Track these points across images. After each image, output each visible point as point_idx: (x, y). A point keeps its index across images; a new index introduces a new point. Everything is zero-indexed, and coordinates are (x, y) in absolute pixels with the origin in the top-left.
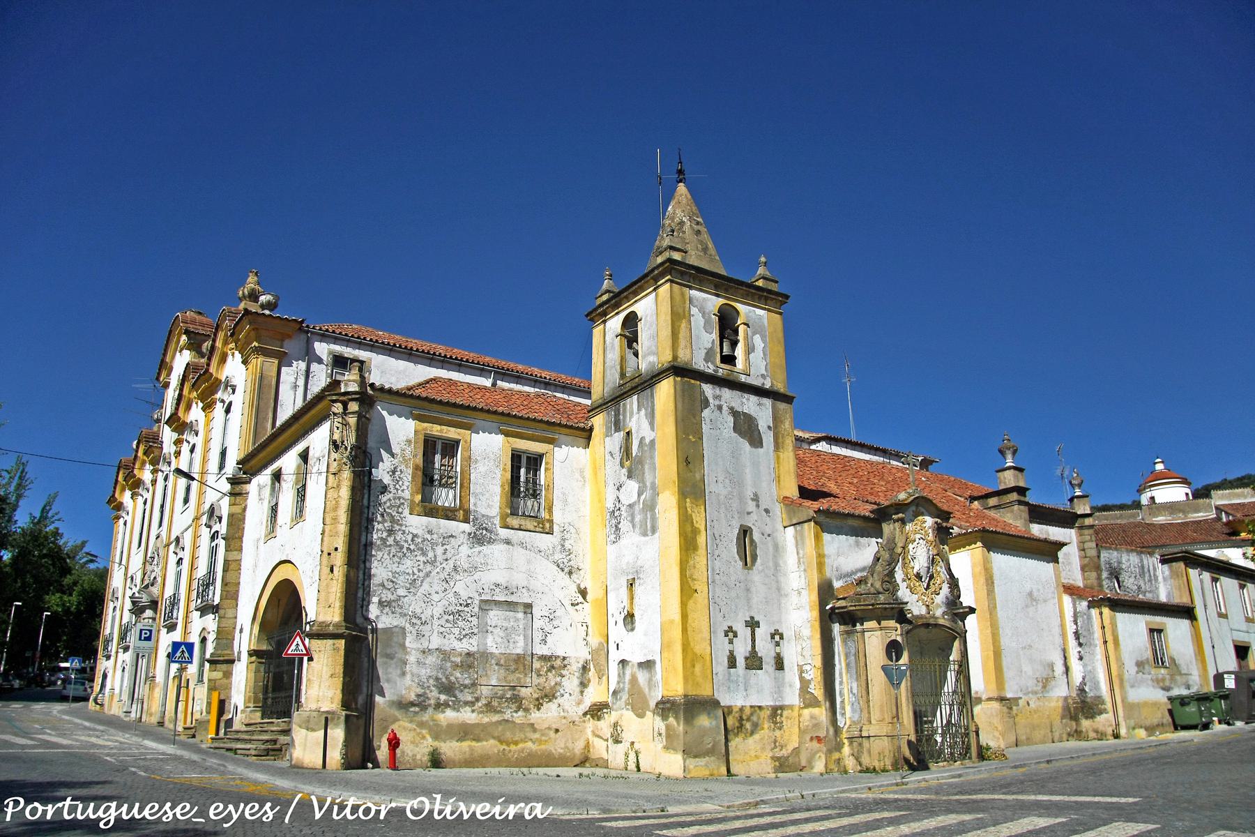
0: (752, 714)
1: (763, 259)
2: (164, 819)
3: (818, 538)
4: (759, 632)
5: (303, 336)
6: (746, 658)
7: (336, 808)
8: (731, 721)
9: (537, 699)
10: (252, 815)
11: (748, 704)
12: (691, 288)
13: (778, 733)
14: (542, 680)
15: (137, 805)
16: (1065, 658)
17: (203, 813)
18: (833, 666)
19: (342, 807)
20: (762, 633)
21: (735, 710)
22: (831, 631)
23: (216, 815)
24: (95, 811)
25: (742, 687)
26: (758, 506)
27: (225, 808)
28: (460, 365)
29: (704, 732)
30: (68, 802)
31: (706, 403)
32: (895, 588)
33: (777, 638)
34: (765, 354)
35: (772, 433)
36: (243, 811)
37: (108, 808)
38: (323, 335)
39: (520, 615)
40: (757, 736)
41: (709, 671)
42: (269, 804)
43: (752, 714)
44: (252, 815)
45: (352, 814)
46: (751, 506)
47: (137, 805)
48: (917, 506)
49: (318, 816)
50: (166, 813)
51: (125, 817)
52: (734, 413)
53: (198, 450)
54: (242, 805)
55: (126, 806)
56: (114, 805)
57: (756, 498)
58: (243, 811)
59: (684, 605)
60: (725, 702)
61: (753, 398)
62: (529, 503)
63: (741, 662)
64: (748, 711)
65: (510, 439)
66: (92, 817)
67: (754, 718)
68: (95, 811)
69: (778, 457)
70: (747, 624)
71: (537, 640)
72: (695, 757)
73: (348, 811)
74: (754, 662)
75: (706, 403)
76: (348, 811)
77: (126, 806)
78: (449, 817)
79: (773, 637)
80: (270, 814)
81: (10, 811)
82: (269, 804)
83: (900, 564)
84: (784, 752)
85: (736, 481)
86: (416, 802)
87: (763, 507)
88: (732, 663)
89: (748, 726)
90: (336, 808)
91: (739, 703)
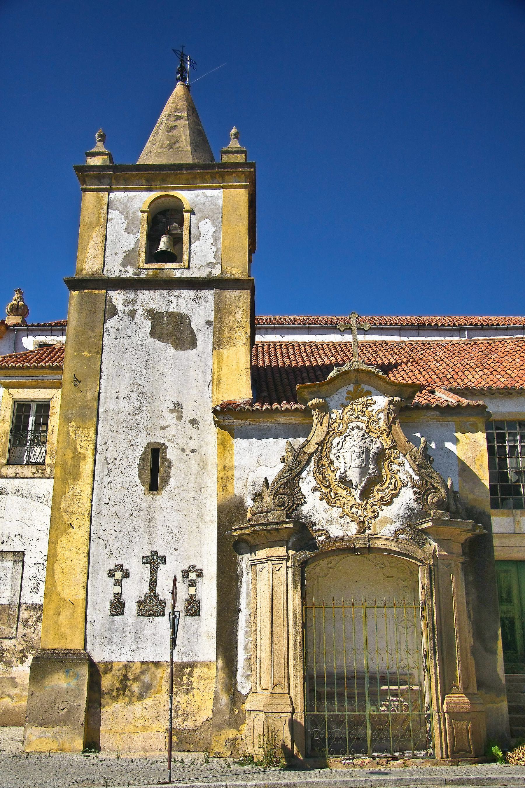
0: (143, 673)
1: (233, 131)
3: (223, 445)
4: (163, 571)
5: (12, 335)
6: (140, 603)
8: (107, 682)
9: (22, 651)
11: (138, 658)
12: (110, 191)
13: (182, 698)
14: (29, 631)
16: (520, 586)
18: (237, 611)
20: (166, 574)
21: (116, 667)
22: (236, 564)
25: (130, 638)
26: (180, 418)
28: (52, 330)
29: (58, 694)
31: (112, 311)
32: (298, 500)
33: (192, 576)
34: (215, 239)
35: (211, 329)
38: (308, 328)
39: (10, 564)
40: (148, 701)
41: (81, 619)
43: (143, 673)
46: (170, 419)
48: (357, 383)
52: (153, 315)
57: (178, 409)
59: (52, 542)
60: (98, 656)
61: (187, 294)
62: (37, 450)
63: (131, 607)
64: (137, 669)
65: (12, 391)
67: (147, 678)
69: (220, 356)
70: (145, 560)
71: (26, 588)
72: (40, 725)
74: (151, 606)
75: (112, 311)
79: (111, 574)
83: (311, 467)
84: (190, 724)
85: (143, 393)
87: (188, 415)
88: (118, 607)
89: (135, 687)
91: (124, 659)
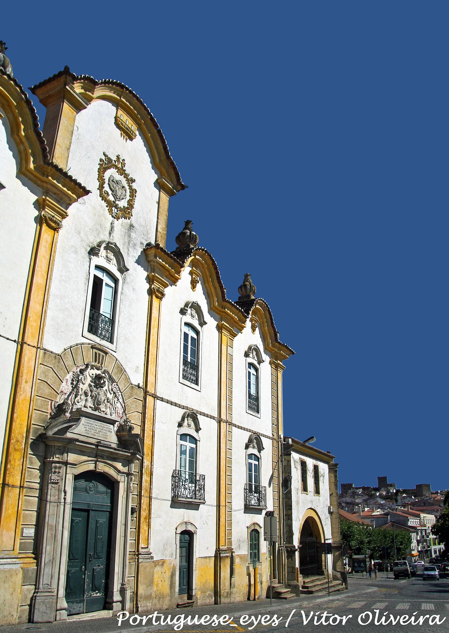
2: (273, 625)
7: (316, 618)
10: (265, 622)
15: (170, 616)
17: (236, 620)
19: (320, 618)
23: (404, 622)
24: (172, 620)
27: (250, 618)
30: (155, 614)
36: (260, 620)
37: (180, 618)
42: (276, 616)
44: (265, 622)
45: (326, 622)
47: (170, 616)
49: (305, 623)
50: (214, 621)
51: (190, 624)
53: (238, 500)
54: (399, 617)
55: (190, 617)
56: (183, 616)
58: (260, 620)
66: (170, 623)
68: (172, 620)
73: (323, 620)
76: (323, 620)
77: (190, 617)
78: (384, 624)
80: (277, 622)
81: (120, 620)
82: (276, 616)
86: (364, 614)
90: (316, 618)
